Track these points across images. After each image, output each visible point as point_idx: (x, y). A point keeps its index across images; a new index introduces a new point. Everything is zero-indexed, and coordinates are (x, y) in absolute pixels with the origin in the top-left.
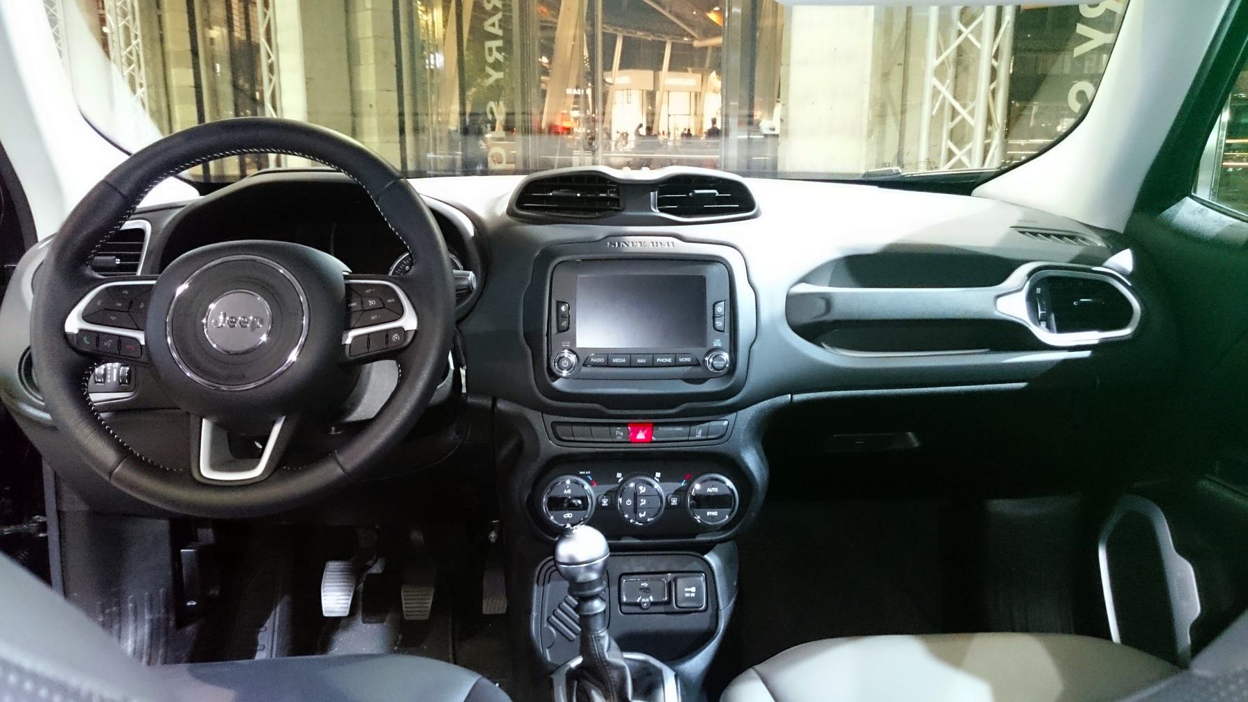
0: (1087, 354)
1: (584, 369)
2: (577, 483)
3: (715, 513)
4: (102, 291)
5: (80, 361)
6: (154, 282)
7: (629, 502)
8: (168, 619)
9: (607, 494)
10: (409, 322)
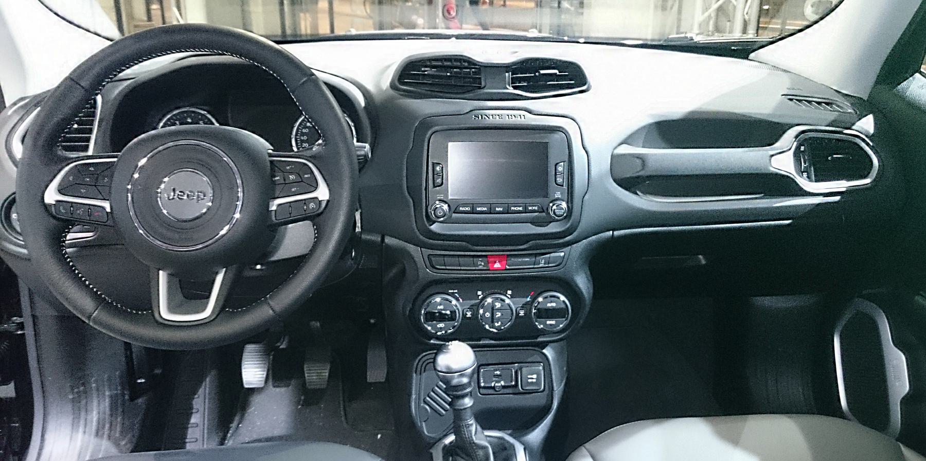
0: (837, 198)
1: (454, 215)
2: (447, 300)
3: (553, 322)
4: (71, 169)
5: (60, 223)
6: (115, 160)
7: (488, 315)
8: (123, 395)
9: (471, 308)
10: (322, 193)
